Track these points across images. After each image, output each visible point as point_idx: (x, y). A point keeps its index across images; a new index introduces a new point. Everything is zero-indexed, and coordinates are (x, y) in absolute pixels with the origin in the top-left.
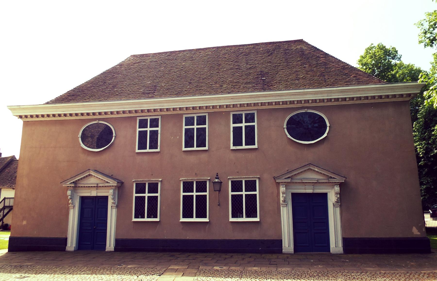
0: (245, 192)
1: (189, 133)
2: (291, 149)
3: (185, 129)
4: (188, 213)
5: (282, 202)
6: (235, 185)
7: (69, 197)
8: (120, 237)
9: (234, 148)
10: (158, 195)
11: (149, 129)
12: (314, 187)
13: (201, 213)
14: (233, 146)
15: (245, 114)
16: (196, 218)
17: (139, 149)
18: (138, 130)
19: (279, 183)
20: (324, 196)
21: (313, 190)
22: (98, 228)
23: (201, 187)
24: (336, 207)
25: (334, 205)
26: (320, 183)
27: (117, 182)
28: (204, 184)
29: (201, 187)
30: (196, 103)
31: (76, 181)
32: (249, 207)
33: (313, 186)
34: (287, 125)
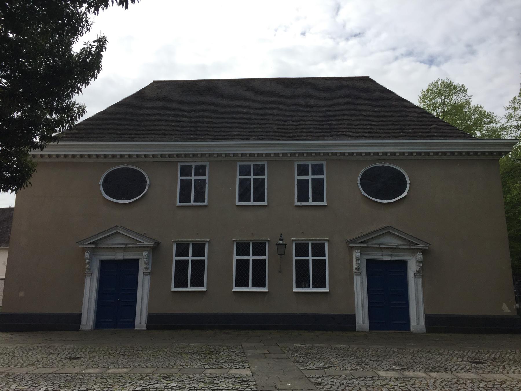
0: (312, 256)
1: (244, 184)
4: (242, 281)
5: (355, 270)
7: (87, 261)
9: (299, 204)
10: (205, 258)
11: (193, 178)
13: (259, 282)
14: (298, 201)
15: (312, 164)
16: (252, 287)
17: (239, 201)
18: (179, 178)
19: (352, 248)
20: (404, 264)
23: (259, 249)
24: (146, 275)
25: (415, 275)
26: (399, 248)
27: (154, 243)
29: (259, 249)
30: (273, 149)
31: (97, 240)
33: (391, 252)
34: (361, 179)
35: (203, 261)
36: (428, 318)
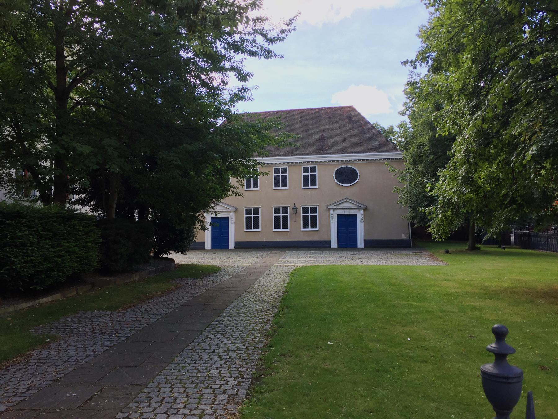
23: (285, 210)
35: (259, 217)
36: (235, 243)
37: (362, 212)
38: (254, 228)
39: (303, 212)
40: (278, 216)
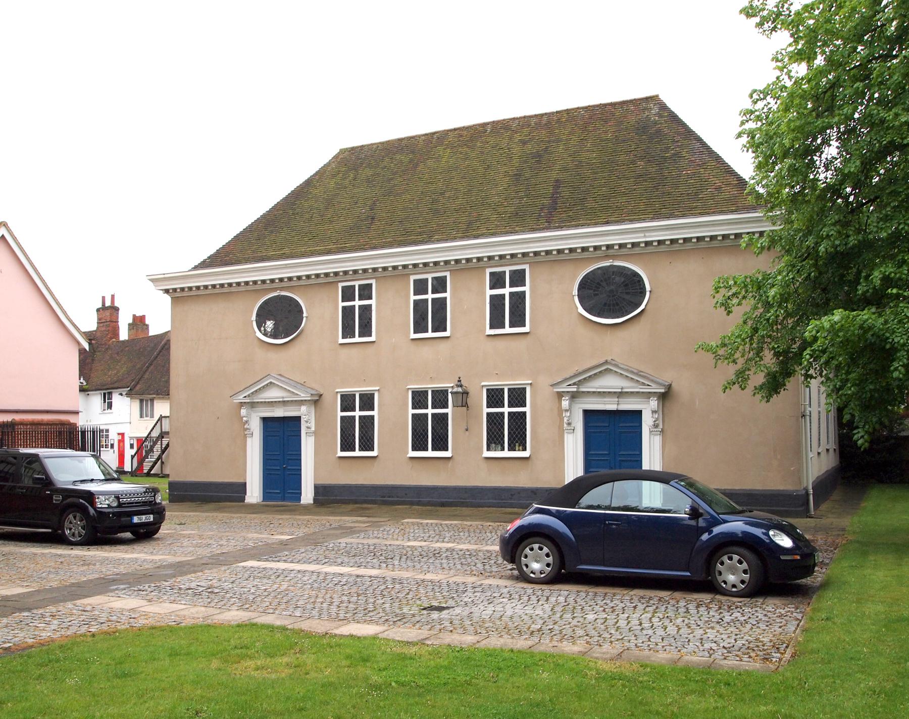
2: (584, 333)
3: (414, 301)
6: (493, 396)
8: (322, 482)
12: (620, 400)
16: (509, 450)
17: (415, 333)
18: (413, 298)
21: (618, 404)
22: (289, 468)
23: (440, 398)
24: (309, 436)
25: (651, 432)
28: (521, 393)
32: (514, 433)
36: (317, 488)
37: (654, 403)
38: (361, 449)
39: (488, 402)
40: (497, 413)
